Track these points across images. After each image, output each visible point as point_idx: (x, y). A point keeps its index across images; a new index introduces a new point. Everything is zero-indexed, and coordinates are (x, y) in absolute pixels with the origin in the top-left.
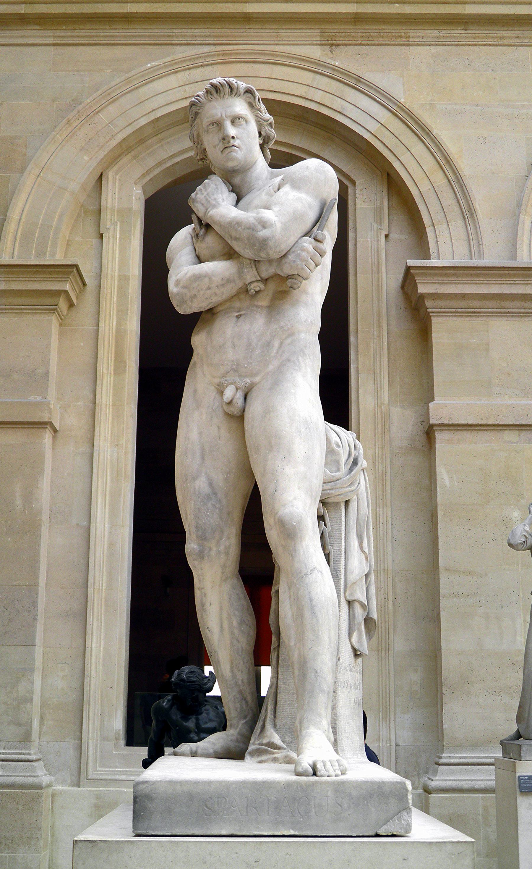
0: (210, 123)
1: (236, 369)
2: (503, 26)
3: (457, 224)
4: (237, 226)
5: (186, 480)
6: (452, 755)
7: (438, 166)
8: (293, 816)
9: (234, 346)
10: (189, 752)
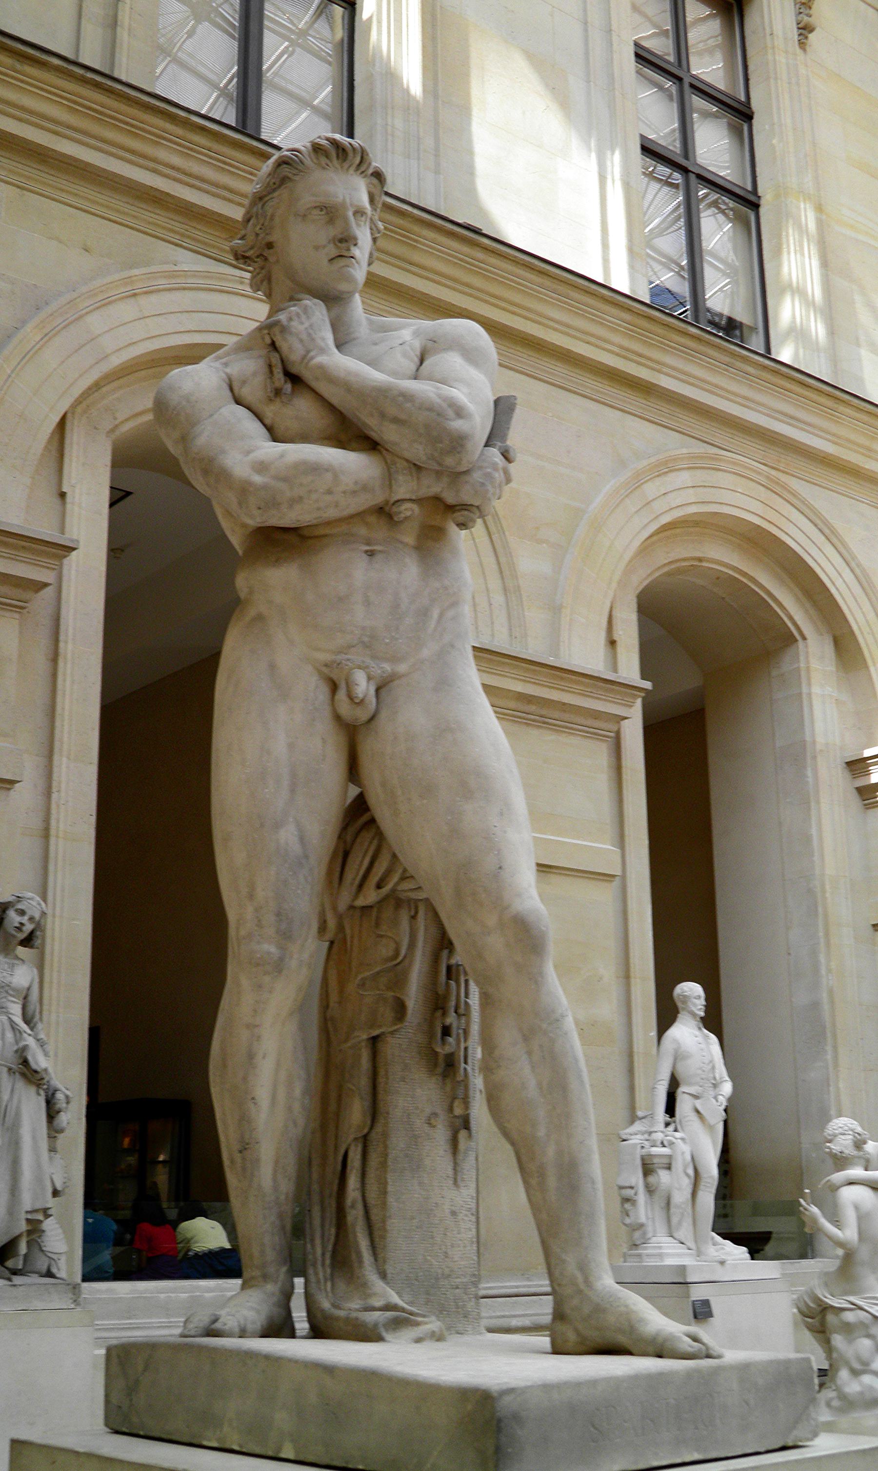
0: (318, 204)
1: (368, 642)
5: (262, 826)
9: (367, 603)
10: (237, 1330)
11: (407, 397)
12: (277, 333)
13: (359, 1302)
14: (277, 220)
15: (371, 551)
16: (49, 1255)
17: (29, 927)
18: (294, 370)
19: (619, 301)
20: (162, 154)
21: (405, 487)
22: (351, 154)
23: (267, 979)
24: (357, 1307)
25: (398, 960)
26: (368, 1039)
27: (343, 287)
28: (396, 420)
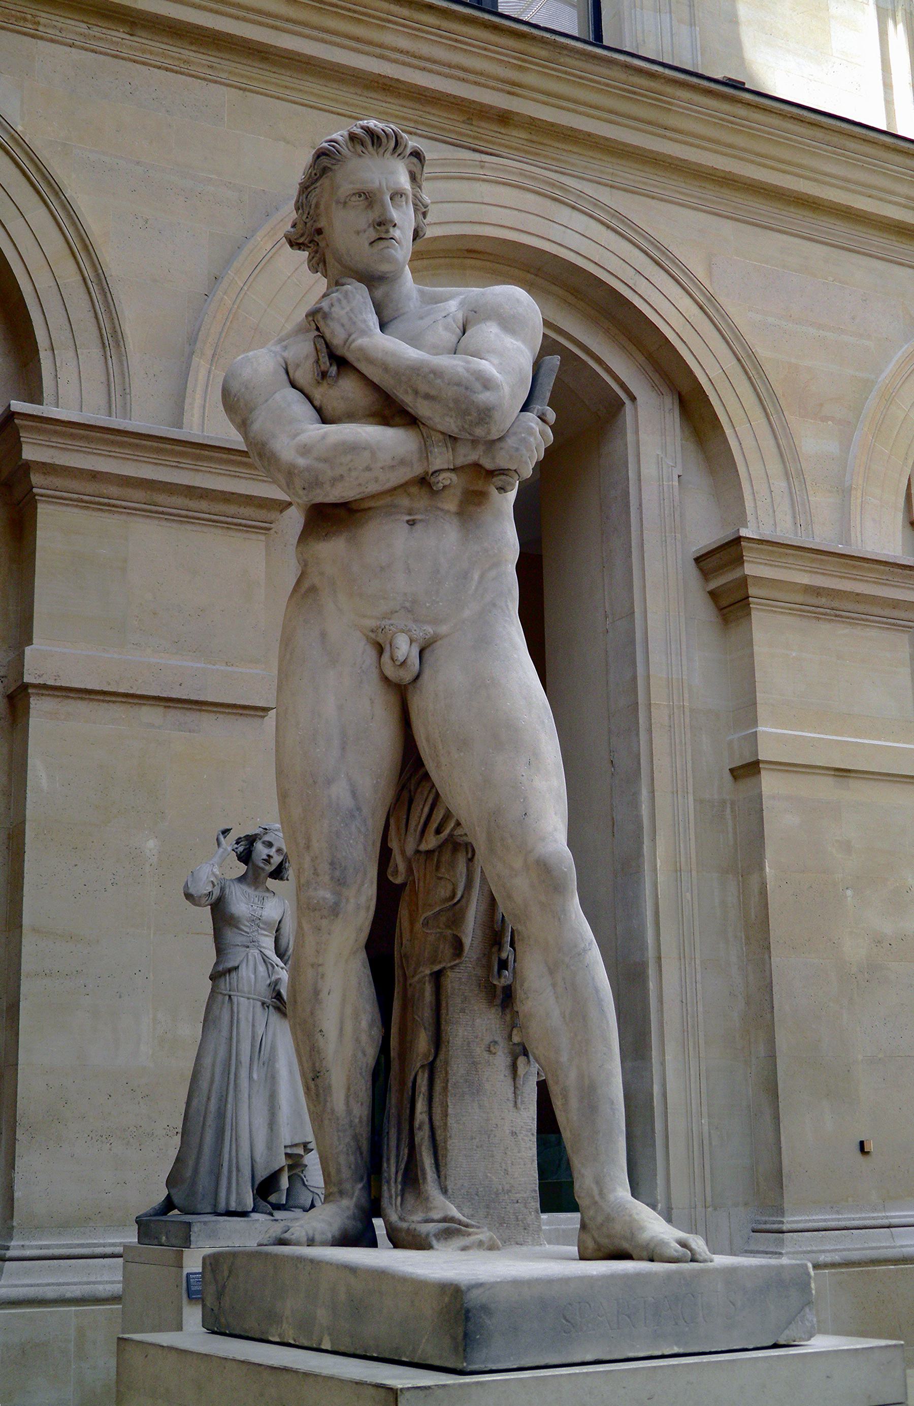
1: (411, 608)
2: (191, 43)
3: (92, 353)
4: (432, 376)
5: (315, 783)
6: (27, 1243)
7: (67, 251)
8: (677, 1324)
9: (408, 571)
11: (437, 373)
12: (320, 319)
13: (421, 1214)
14: (322, 207)
15: (413, 520)
16: (312, 1189)
17: (277, 860)
18: (339, 352)
19: (903, 147)
20: (389, 38)
21: (441, 458)
22: (384, 140)
23: (324, 923)
24: (419, 1219)
25: (456, 900)
26: (431, 974)
27: (384, 268)
28: (427, 397)
